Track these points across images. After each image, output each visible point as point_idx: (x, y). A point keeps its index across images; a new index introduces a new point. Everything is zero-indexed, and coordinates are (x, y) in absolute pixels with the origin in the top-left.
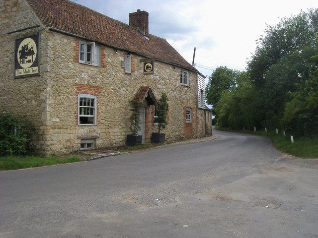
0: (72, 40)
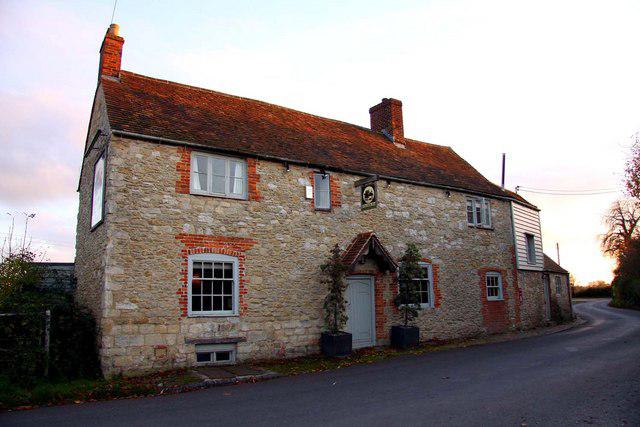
0: (172, 151)
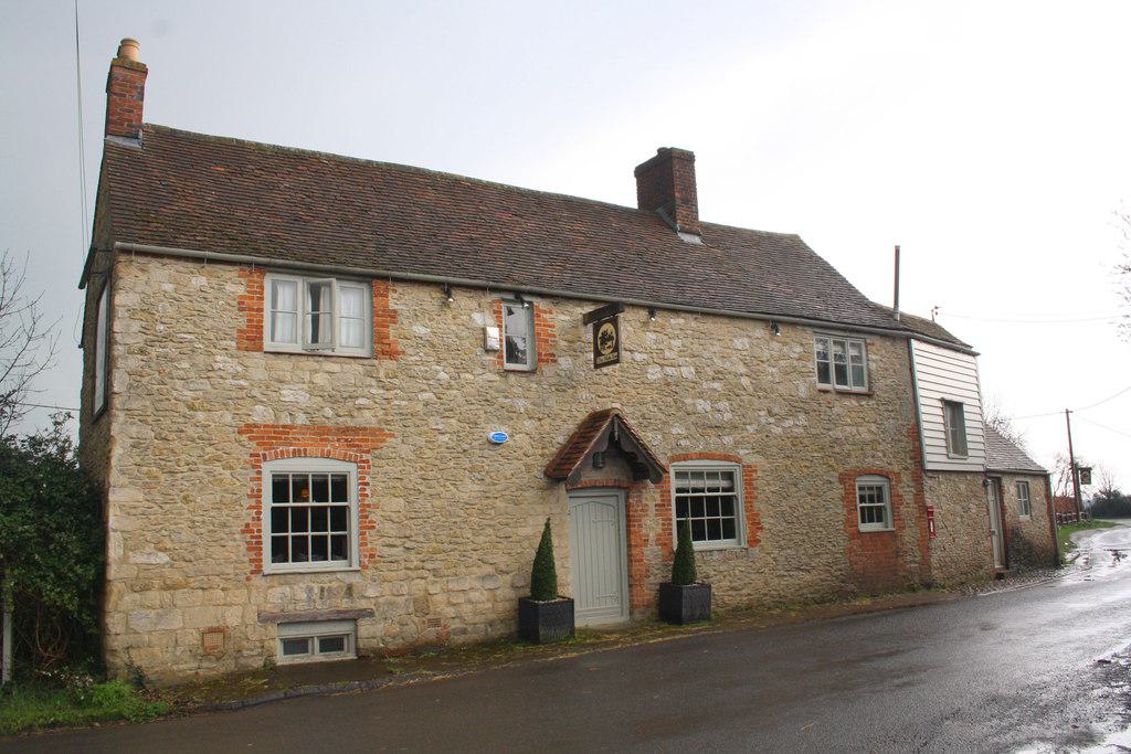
0: (228, 275)
